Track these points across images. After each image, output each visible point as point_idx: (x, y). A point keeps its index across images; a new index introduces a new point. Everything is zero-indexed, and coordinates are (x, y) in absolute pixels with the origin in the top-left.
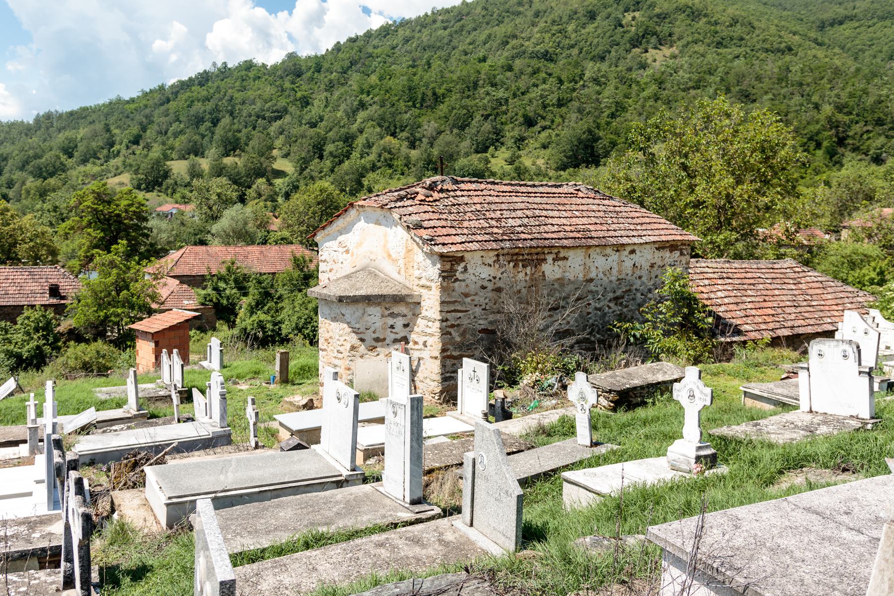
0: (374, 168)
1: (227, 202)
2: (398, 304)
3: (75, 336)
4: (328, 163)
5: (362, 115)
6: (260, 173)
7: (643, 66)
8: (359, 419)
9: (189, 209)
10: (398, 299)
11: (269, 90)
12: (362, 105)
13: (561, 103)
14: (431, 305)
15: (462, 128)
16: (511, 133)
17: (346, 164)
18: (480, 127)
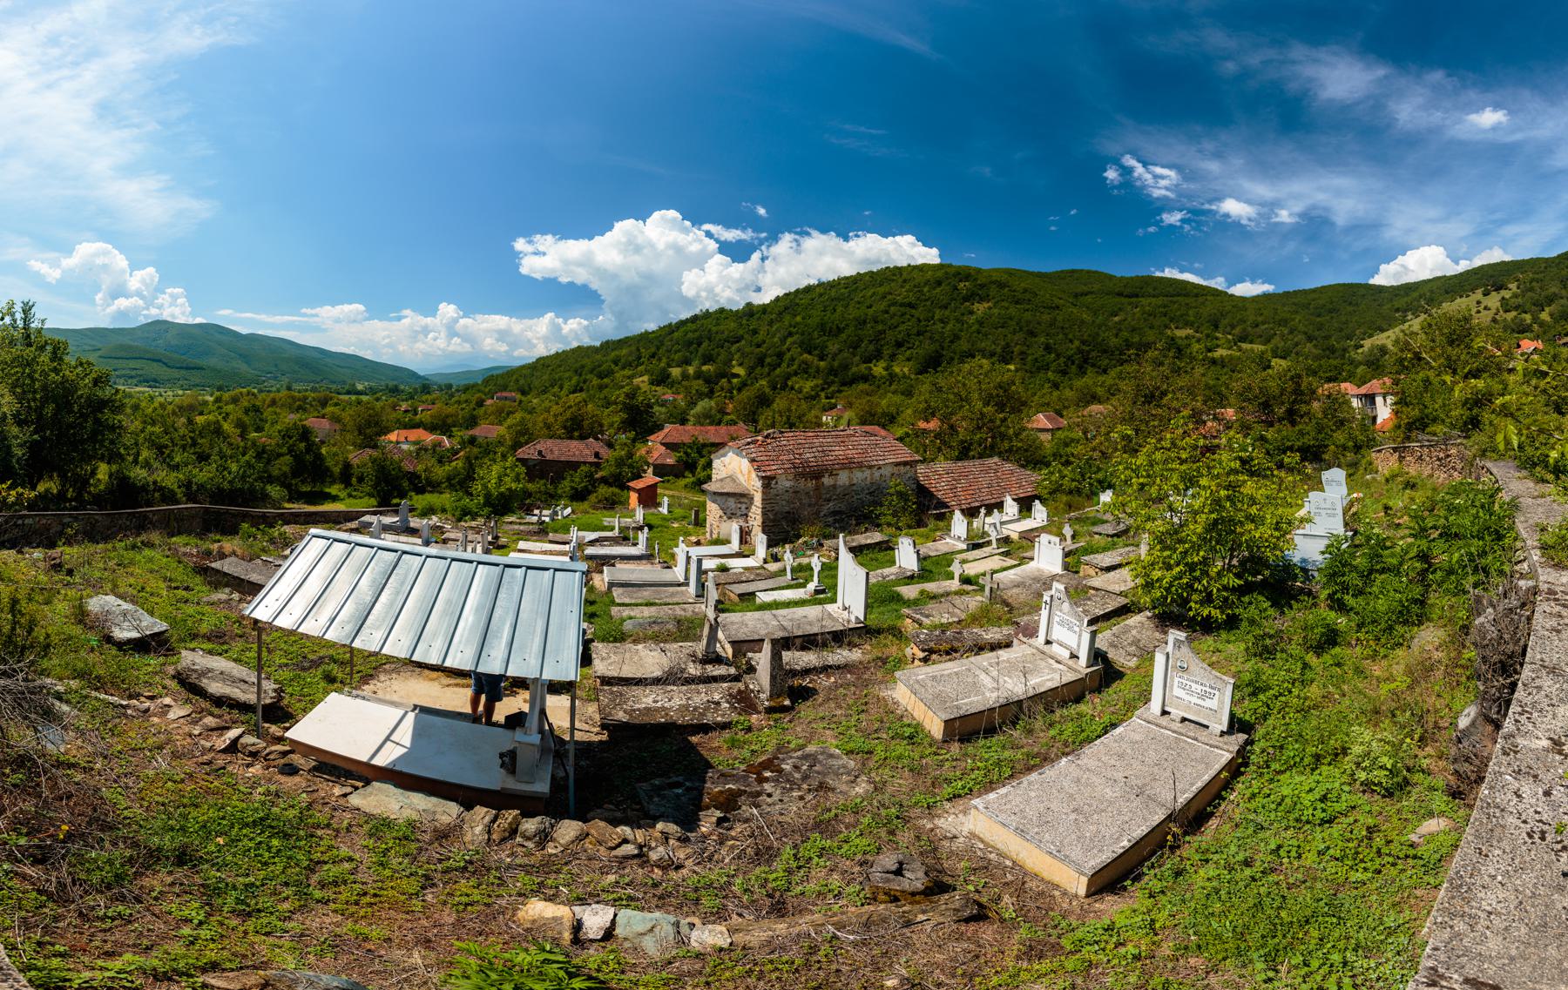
0: (796, 374)
1: (701, 395)
2: (743, 497)
3: (604, 480)
4: (766, 370)
5: (790, 340)
6: (723, 375)
7: (971, 313)
8: (468, 709)
9: (680, 397)
10: (743, 495)
11: (733, 325)
12: (790, 334)
13: (919, 334)
14: (758, 499)
15: (855, 348)
16: (887, 352)
17: (778, 371)
18: (867, 347)
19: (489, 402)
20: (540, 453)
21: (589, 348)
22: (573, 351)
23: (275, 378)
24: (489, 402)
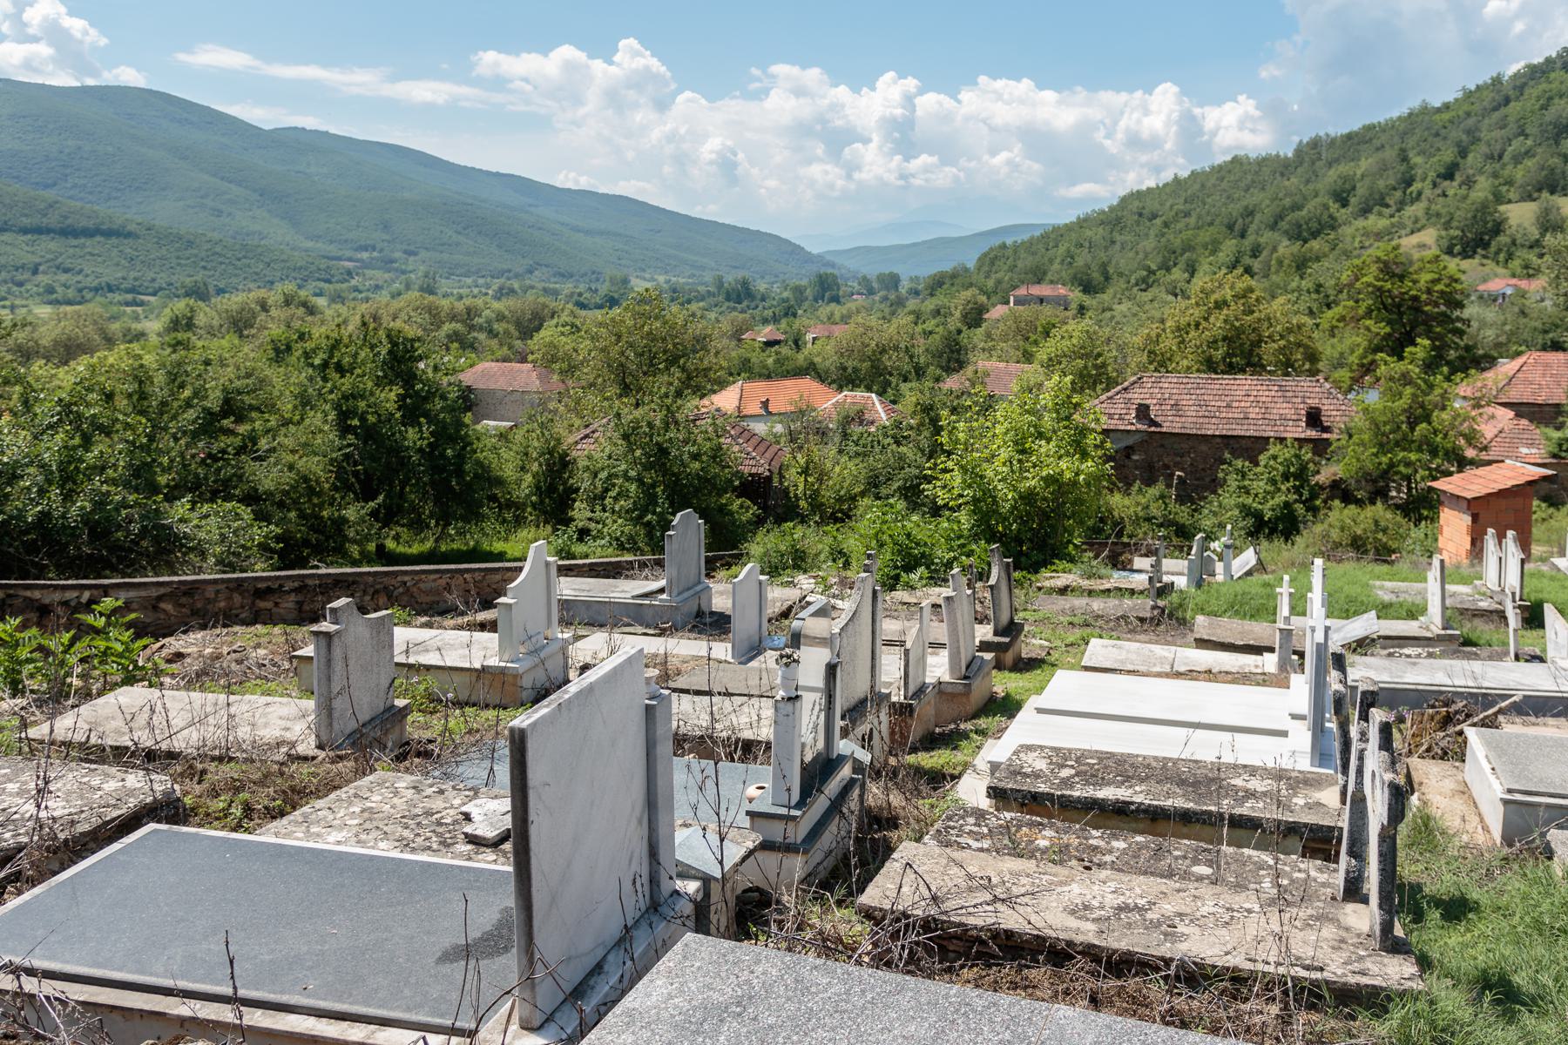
19: (997, 312)
20: (1143, 412)
21: (1263, 162)
22: (1221, 171)
23: (387, 263)
24: (997, 312)
